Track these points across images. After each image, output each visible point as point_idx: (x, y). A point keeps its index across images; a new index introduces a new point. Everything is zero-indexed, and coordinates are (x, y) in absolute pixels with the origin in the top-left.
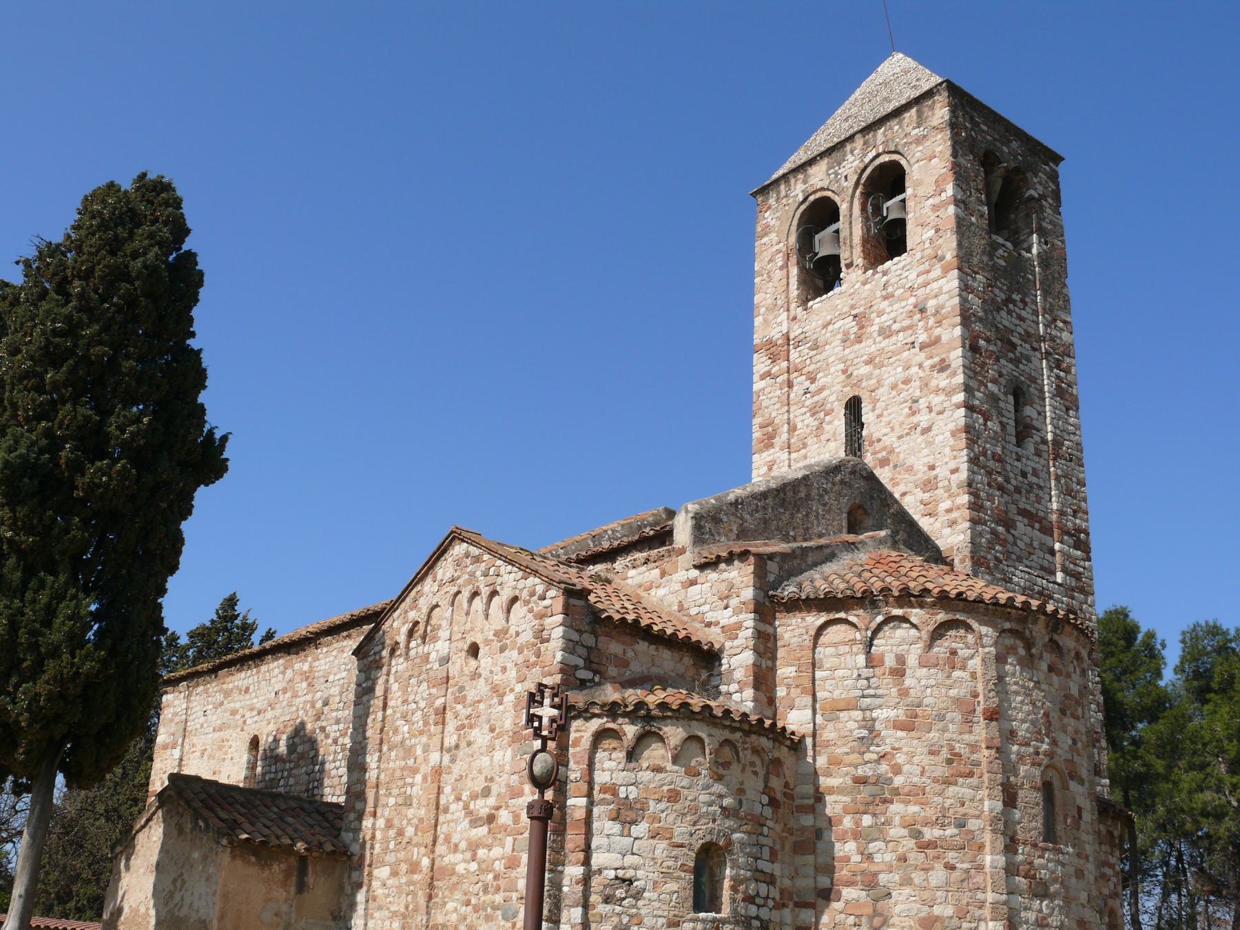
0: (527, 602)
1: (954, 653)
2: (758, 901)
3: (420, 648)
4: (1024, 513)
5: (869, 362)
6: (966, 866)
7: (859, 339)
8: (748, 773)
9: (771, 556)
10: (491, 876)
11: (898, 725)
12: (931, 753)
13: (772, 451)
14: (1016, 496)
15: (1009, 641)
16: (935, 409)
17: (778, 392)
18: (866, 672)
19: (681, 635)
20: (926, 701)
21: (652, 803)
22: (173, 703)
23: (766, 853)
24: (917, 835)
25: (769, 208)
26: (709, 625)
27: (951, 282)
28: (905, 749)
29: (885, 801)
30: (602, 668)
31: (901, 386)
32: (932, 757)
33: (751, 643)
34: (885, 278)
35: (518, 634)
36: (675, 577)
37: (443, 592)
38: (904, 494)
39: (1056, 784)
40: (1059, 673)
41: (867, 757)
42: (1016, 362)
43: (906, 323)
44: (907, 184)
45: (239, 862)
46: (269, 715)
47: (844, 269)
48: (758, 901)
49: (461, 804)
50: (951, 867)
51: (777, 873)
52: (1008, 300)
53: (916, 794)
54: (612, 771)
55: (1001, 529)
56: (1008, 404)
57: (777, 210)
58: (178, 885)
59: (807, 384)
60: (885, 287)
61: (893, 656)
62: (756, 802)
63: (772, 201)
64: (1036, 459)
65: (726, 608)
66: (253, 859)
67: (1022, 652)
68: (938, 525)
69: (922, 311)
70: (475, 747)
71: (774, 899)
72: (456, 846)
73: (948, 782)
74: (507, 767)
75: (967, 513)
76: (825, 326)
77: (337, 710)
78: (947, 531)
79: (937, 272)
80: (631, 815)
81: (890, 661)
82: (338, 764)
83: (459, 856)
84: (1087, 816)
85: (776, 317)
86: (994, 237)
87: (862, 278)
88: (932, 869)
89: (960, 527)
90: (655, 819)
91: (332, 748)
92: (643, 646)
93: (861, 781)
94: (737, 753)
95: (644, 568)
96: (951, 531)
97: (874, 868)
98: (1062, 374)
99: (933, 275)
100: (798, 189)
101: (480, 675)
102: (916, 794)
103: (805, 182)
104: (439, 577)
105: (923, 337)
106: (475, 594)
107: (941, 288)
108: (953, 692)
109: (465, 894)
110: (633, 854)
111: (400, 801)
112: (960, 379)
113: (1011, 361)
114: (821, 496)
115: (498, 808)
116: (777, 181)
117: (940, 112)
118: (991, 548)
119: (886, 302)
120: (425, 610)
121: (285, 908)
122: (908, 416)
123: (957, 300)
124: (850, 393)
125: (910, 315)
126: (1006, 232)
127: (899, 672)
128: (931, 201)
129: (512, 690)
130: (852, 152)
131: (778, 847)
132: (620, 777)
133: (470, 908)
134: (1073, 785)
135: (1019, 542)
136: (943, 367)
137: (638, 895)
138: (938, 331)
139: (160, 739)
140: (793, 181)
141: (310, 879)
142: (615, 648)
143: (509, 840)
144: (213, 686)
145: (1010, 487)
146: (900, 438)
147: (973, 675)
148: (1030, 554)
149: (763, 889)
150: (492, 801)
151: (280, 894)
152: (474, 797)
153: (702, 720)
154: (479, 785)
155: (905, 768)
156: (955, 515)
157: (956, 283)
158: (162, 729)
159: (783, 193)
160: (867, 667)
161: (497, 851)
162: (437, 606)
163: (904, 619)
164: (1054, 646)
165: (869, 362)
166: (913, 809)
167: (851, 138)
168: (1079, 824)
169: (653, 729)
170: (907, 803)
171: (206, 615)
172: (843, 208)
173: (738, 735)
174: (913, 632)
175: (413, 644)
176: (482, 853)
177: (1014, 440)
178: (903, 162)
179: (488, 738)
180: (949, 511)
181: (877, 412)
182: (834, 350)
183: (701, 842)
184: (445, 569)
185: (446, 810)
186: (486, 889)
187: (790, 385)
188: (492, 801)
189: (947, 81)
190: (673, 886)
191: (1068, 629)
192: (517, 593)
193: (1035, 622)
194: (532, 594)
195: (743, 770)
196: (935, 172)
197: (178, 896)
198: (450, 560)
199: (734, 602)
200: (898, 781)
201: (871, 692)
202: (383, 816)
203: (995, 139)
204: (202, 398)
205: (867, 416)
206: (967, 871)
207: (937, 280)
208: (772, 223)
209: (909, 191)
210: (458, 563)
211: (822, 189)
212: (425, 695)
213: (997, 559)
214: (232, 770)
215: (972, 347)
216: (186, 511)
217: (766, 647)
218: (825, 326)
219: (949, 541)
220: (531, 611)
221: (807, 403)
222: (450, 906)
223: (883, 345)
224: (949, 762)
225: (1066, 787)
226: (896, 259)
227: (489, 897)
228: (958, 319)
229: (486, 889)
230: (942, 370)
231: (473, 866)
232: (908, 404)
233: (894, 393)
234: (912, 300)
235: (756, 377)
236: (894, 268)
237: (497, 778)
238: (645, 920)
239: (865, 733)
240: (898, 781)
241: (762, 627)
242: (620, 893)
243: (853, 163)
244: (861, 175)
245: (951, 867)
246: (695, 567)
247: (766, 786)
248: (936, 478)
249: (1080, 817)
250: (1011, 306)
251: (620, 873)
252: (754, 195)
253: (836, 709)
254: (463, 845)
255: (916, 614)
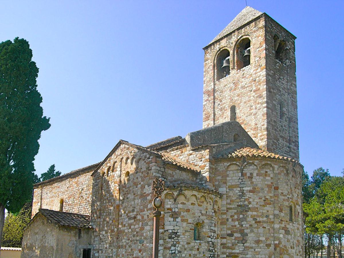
0: (144, 160)
1: (266, 172)
2: (211, 237)
3: (111, 174)
4: (281, 137)
5: (238, 95)
6: (269, 227)
7: (235, 89)
8: (209, 204)
9: (214, 147)
10: (135, 233)
11: (250, 191)
12: (260, 198)
13: (209, 121)
14: (280, 132)
15: (282, 169)
16: (258, 108)
17: (210, 105)
18: (242, 178)
19: (189, 168)
20: (258, 185)
21: (182, 213)
22: (37, 192)
23: (213, 225)
24: (255, 219)
25: (208, 53)
26: (196, 166)
27: (264, 73)
28: (252, 198)
29: (246, 211)
30: (167, 177)
31: (247, 102)
32: (259, 200)
33: (208, 170)
34: (243, 72)
35: (141, 168)
36: (185, 153)
37: (117, 158)
38: (55, 209)
39: (293, 206)
40: (295, 177)
41: (241, 200)
42: (281, 95)
43: (249, 85)
44: (251, 45)
45: (61, 231)
46: (66, 193)
47: (231, 70)
48: (211, 237)
49: (126, 214)
50: (264, 227)
51: (216, 230)
52: (280, 78)
53: (256, 209)
54: (170, 204)
55: (276, 141)
56: (278, 107)
57: (210, 53)
58: (44, 237)
59: (219, 102)
60: (243, 75)
61: (249, 173)
62: (210, 212)
63: (209, 51)
64: (285, 122)
65: (201, 161)
66: (65, 230)
67: (285, 172)
68: (257, 140)
69: (255, 81)
70: (129, 199)
71: (215, 236)
72: (125, 225)
73: (263, 206)
74: (139, 204)
75: (266, 137)
76: (225, 86)
77: (86, 191)
78: (260, 141)
79: (259, 70)
80: (175, 216)
81: (248, 175)
82: (87, 205)
83: (126, 228)
84: (300, 214)
85: (210, 84)
86: (276, 60)
87: (236, 72)
88: (259, 228)
89: (264, 140)
90: (183, 216)
91: (85, 201)
92: (178, 171)
93: (238, 206)
94: (206, 199)
95: (176, 151)
96: (261, 141)
97: (242, 228)
98: (293, 99)
99: (258, 71)
100: (217, 47)
101: (130, 180)
102: (256, 209)
103: (219, 45)
104: (116, 154)
105: (254, 88)
106: (128, 158)
107: (261, 74)
108: (266, 183)
109: (128, 237)
110: (177, 226)
111: (107, 214)
112: (265, 100)
113: (279, 95)
114: (226, 131)
115: (137, 215)
116: (210, 45)
117: (262, 23)
118: (272, 146)
119: (243, 79)
120: (112, 163)
121: (75, 242)
122: (250, 110)
123: (265, 78)
124: (232, 104)
125: (251, 82)
126: (279, 59)
127: (251, 177)
128: (258, 49)
129: (140, 184)
130: (234, 35)
131: (216, 223)
132: (172, 206)
133: (129, 241)
134: (297, 206)
135: (280, 145)
136: (260, 96)
137: (178, 236)
138: (259, 87)
139: (34, 201)
140: (215, 45)
141: (82, 235)
142: (170, 172)
143: (141, 223)
144: (48, 187)
145: (278, 130)
146: (247, 116)
147: (272, 178)
148: (283, 147)
149: (213, 234)
150: (135, 213)
151: (74, 239)
152: (129, 212)
153: (196, 190)
154: (131, 209)
155: (252, 203)
156: (262, 137)
157: (265, 73)
158: (34, 198)
159: (212, 48)
160: (241, 176)
161: (137, 226)
162: (116, 162)
163: (253, 163)
164: (294, 171)
165: (238, 95)
166: (255, 213)
167: (234, 32)
168: (298, 216)
169: (182, 193)
170: (253, 211)
171: (46, 170)
172: (231, 52)
173: (206, 194)
174: (255, 167)
175: (109, 172)
176: (132, 227)
177: (279, 117)
178: (250, 38)
179: (133, 197)
180: (261, 136)
181: (240, 110)
182: (227, 93)
183: (196, 222)
184: (118, 152)
185: (121, 216)
186: (134, 236)
187: (214, 103)
188: (135, 213)
189: (265, 13)
190: (187, 234)
191: (298, 166)
192: (141, 157)
193: (289, 164)
194: (146, 157)
195: (207, 204)
196: (260, 41)
197: (44, 240)
198: (119, 149)
199: (203, 159)
200: (250, 206)
201: (243, 183)
202: (102, 218)
203: (277, 31)
204: (41, 105)
205: (237, 111)
206: (269, 229)
207: (259, 72)
208: (209, 57)
209: (251, 47)
210: (122, 150)
211: (225, 47)
212: (113, 186)
213: (274, 148)
214: (109, 182)
215: (269, 90)
216: (39, 137)
217: (213, 171)
218: (225, 86)
219: (261, 144)
220: (145, 162)
221: (219, 108)
222: (123, 241)
223: (242, 91)
224: (264, 201)
225: (295, 207)
226: (247, 67)
227: (135, 238)
228: (265, 83)
229: (134, 236)
230: (260, 97)
231: (130, 230)
232: (250, 107)
233: (245, 104)
234: (251, 78)
235: (204, 101)
236: (246, 69)
237: (136, 207)
238: (181, 243)
239: (241, 194)
240: (250, 206)
241: (211, 166)
242: (173, 236)
243: (234, 39)
244: (236, 42)
245: (264, 227)
246: (191, 150)
247: (213, 207)
248: (257, 127)
249: (299, 214)
250: (280, 80)
251: (173, 231)
252: (204, 49)
253: (231, 188)
254: (127, 225)
255: (256, 162)
